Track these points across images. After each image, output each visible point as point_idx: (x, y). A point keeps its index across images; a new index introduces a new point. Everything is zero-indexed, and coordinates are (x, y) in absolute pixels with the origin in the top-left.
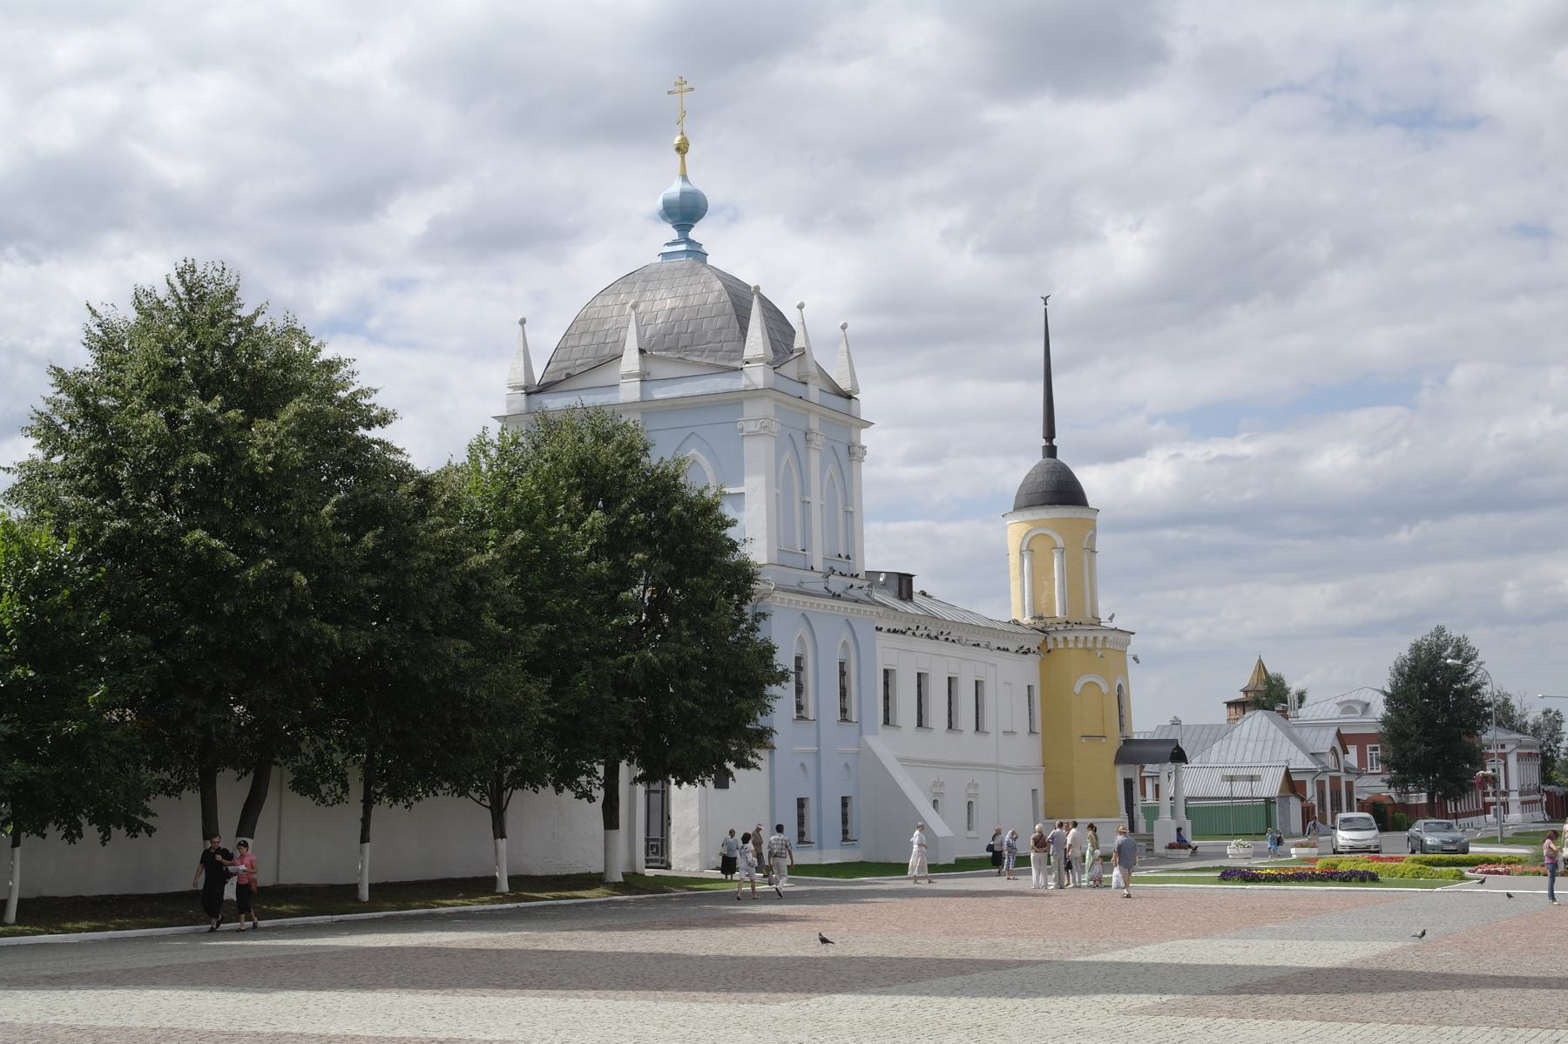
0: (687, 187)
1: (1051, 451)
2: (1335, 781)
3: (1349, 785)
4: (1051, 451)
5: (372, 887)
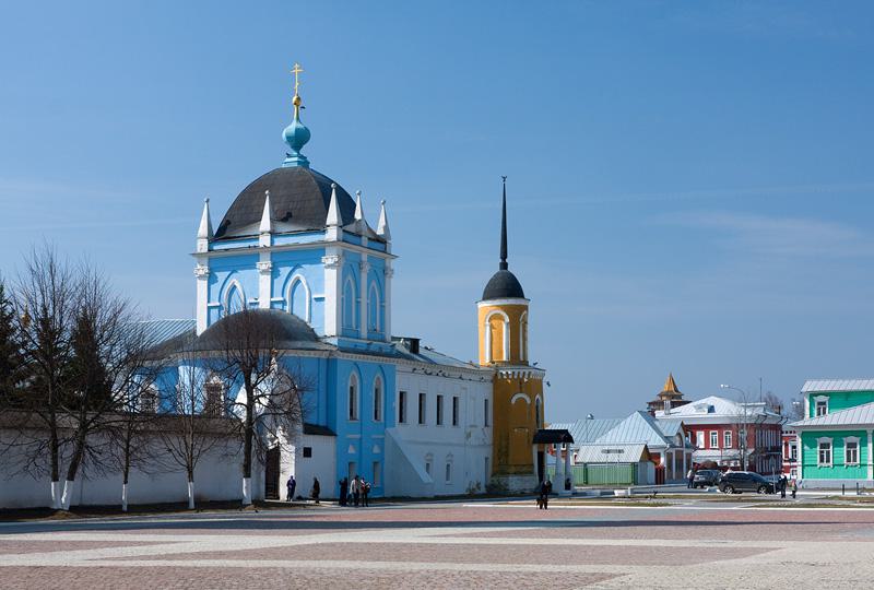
0: (300, 126)
1: (504, 266)
2: (679, 453)
3: (689, 455)
4: (504, 266)
5: (128, 506)
